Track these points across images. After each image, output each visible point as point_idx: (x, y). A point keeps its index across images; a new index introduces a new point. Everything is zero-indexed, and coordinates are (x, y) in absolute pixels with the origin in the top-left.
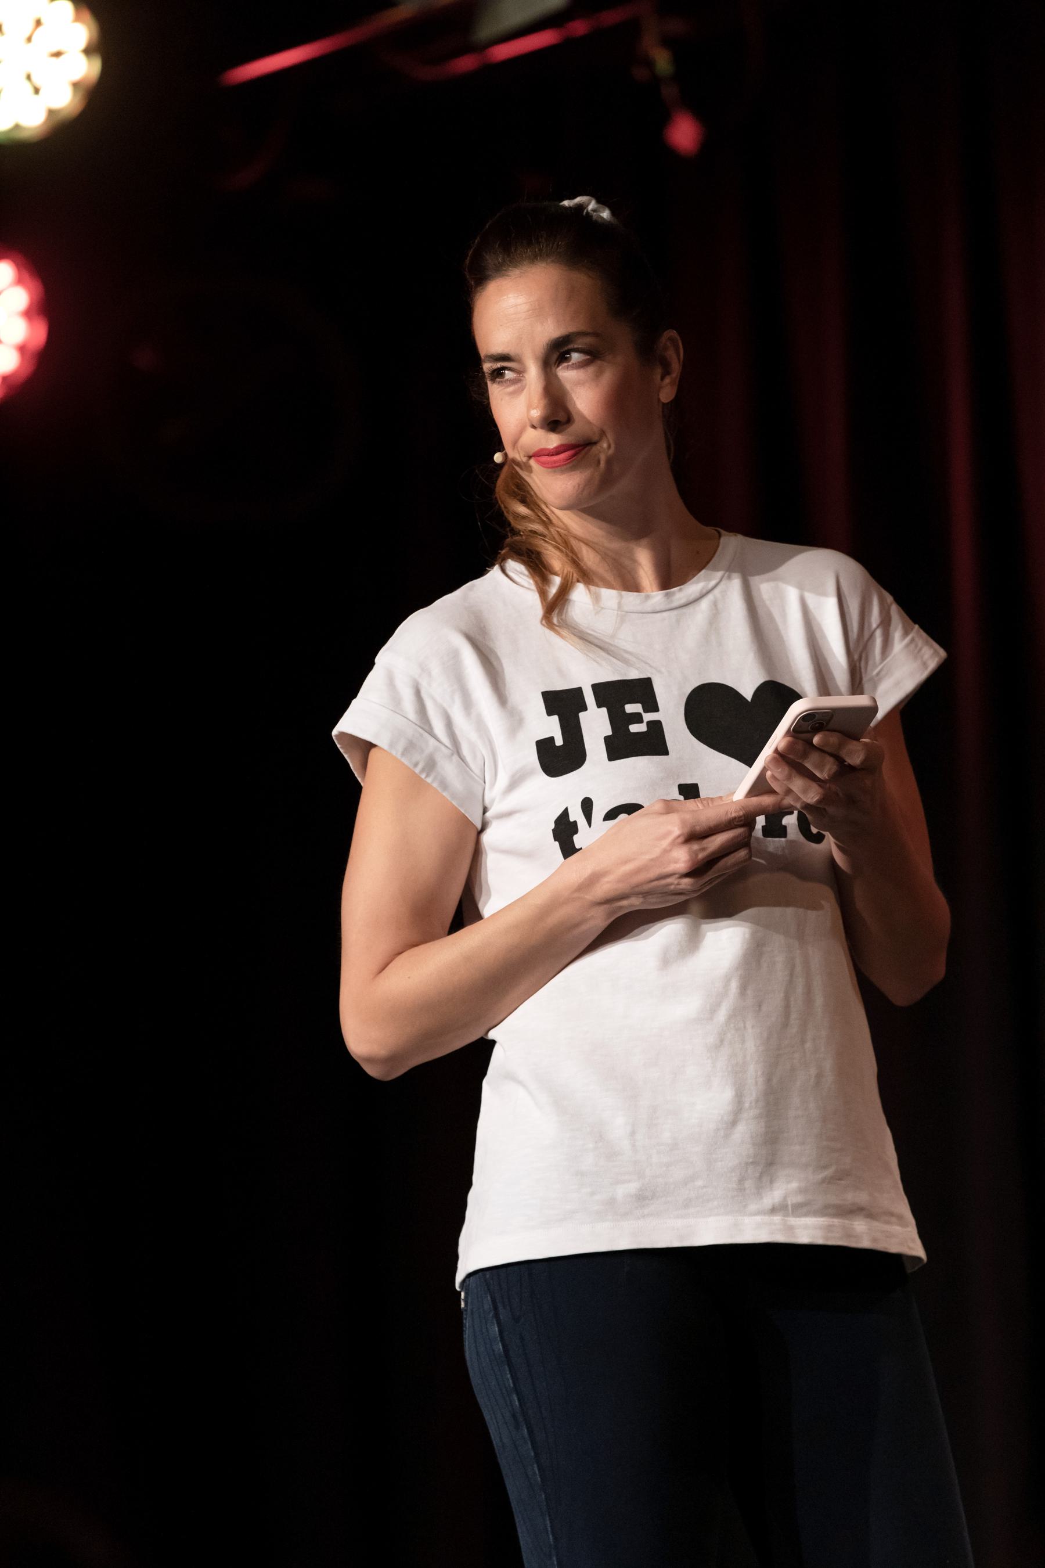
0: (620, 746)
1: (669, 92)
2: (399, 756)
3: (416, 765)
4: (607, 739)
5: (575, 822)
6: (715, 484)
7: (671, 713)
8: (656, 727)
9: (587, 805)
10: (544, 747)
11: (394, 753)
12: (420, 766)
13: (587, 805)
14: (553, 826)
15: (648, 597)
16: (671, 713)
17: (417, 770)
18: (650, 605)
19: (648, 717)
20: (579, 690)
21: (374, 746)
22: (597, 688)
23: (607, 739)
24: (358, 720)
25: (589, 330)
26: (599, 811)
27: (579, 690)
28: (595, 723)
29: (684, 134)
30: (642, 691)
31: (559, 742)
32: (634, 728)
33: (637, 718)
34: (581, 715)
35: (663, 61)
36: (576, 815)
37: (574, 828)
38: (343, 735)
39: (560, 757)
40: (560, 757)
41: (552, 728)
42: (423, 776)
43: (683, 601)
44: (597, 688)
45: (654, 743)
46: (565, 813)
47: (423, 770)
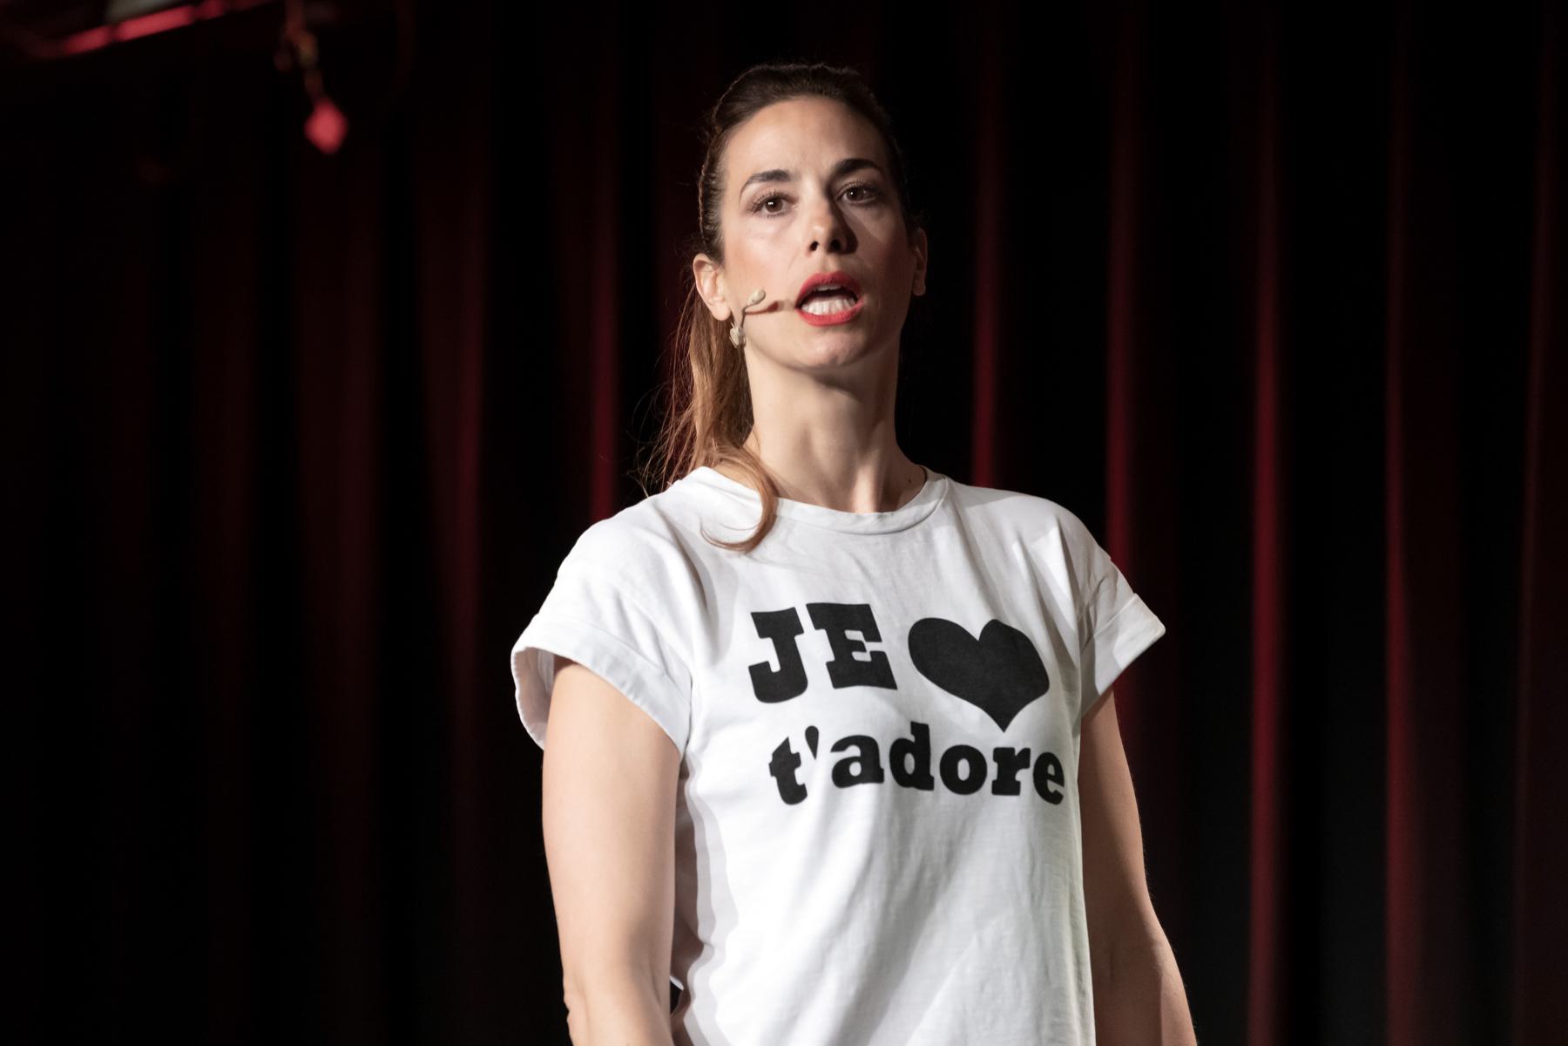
0: (844, 673)
1: (313, 82)
2: (603, 675)
3: (623, 684)
4: (829, 665)
5: (797, 755)
6: (931, 413)
7: (894, 645)
8: (880, 657)
9: (812, 735)
10: (759, 673)
11: (597, 671)
12: (628, 685)
13: (812, 735)
14: (770, 759)
15: (859, 518)
16: (894, 645)
17: (624, 691)
18: (861, 527)
19: (871, 646)
20: (793, 611)
21: (562, 663)
22: (813, 609)
23: (829, 665)
24: (539, 634)
25: (869, 155)
26: (826, 741)
27: (793, 611)
28: (814, 647)
29: (326, 128)
30: (861, 617)
31: (775, 667)
32: (858, 656)
33: (860, 647)
34: (798, 638)
35: (307, 49)
36: (799, 746)
37: (796, 760)
38: (533, 653)
39: (780, 683)
40: (780, 683)
41: (766, 652)
42: (631, 697)
43: (896, 527)
44: (813, 609)
45: (878, 674)
46: (786, 744)
47: (630, 691)
